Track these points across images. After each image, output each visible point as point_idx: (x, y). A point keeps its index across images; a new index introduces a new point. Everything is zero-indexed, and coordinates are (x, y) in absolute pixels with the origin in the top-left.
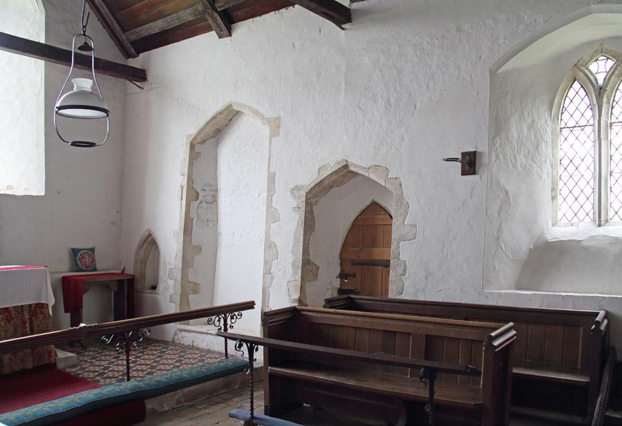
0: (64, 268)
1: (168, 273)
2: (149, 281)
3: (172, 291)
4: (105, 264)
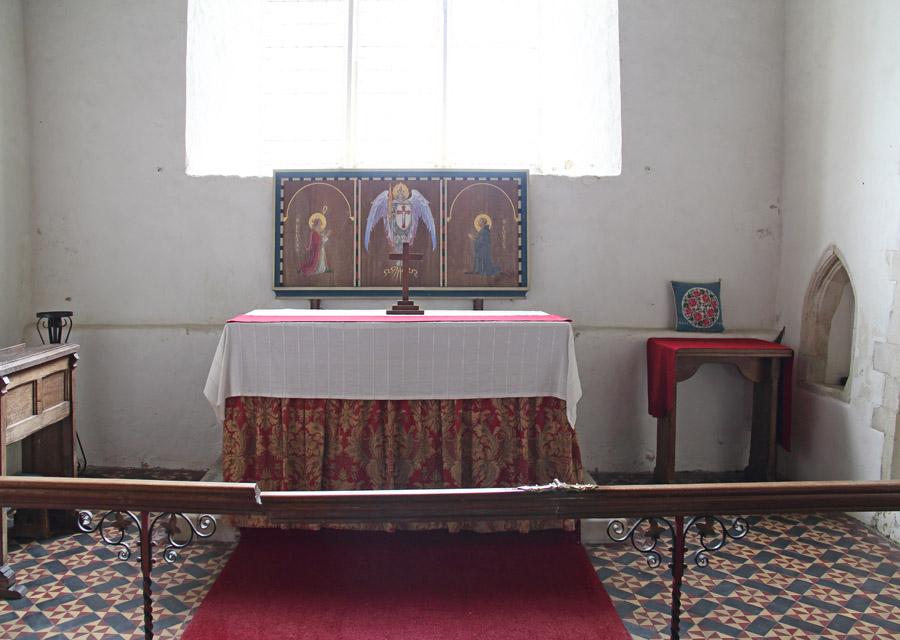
0: (654, 319)
1: (870, 353)
2: (832, 372)
3: (877, 400)
4: (741, 317)
